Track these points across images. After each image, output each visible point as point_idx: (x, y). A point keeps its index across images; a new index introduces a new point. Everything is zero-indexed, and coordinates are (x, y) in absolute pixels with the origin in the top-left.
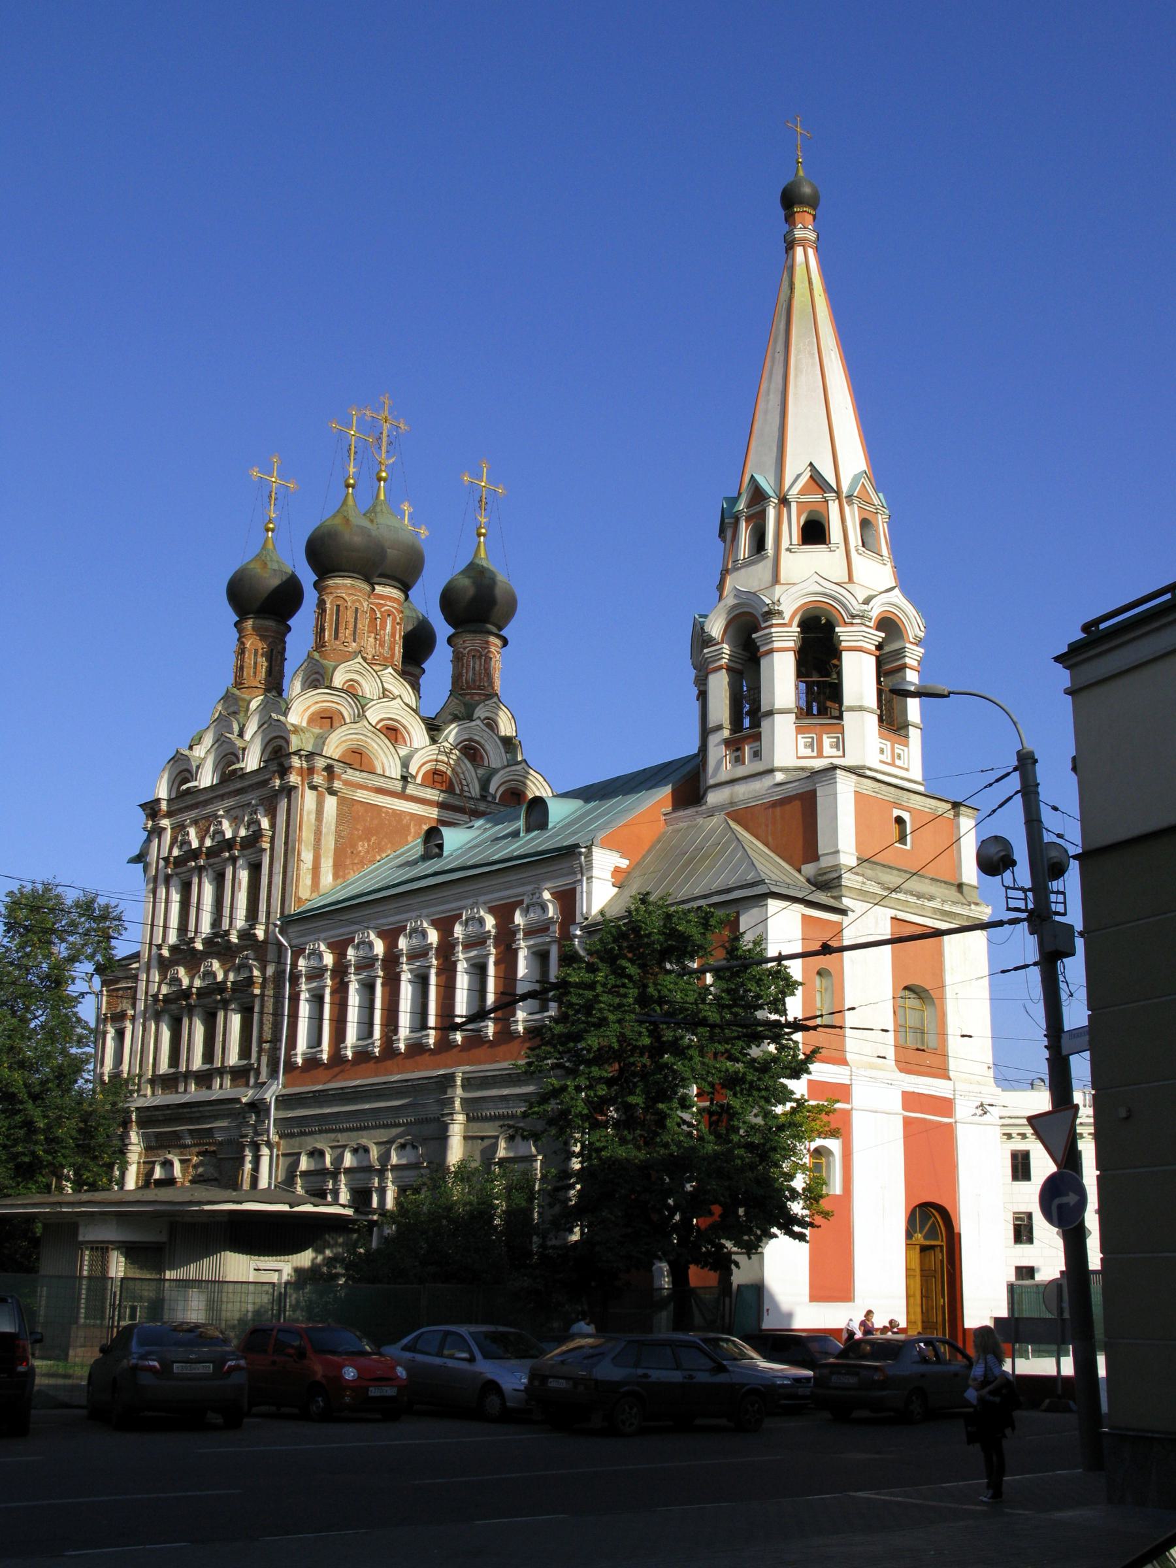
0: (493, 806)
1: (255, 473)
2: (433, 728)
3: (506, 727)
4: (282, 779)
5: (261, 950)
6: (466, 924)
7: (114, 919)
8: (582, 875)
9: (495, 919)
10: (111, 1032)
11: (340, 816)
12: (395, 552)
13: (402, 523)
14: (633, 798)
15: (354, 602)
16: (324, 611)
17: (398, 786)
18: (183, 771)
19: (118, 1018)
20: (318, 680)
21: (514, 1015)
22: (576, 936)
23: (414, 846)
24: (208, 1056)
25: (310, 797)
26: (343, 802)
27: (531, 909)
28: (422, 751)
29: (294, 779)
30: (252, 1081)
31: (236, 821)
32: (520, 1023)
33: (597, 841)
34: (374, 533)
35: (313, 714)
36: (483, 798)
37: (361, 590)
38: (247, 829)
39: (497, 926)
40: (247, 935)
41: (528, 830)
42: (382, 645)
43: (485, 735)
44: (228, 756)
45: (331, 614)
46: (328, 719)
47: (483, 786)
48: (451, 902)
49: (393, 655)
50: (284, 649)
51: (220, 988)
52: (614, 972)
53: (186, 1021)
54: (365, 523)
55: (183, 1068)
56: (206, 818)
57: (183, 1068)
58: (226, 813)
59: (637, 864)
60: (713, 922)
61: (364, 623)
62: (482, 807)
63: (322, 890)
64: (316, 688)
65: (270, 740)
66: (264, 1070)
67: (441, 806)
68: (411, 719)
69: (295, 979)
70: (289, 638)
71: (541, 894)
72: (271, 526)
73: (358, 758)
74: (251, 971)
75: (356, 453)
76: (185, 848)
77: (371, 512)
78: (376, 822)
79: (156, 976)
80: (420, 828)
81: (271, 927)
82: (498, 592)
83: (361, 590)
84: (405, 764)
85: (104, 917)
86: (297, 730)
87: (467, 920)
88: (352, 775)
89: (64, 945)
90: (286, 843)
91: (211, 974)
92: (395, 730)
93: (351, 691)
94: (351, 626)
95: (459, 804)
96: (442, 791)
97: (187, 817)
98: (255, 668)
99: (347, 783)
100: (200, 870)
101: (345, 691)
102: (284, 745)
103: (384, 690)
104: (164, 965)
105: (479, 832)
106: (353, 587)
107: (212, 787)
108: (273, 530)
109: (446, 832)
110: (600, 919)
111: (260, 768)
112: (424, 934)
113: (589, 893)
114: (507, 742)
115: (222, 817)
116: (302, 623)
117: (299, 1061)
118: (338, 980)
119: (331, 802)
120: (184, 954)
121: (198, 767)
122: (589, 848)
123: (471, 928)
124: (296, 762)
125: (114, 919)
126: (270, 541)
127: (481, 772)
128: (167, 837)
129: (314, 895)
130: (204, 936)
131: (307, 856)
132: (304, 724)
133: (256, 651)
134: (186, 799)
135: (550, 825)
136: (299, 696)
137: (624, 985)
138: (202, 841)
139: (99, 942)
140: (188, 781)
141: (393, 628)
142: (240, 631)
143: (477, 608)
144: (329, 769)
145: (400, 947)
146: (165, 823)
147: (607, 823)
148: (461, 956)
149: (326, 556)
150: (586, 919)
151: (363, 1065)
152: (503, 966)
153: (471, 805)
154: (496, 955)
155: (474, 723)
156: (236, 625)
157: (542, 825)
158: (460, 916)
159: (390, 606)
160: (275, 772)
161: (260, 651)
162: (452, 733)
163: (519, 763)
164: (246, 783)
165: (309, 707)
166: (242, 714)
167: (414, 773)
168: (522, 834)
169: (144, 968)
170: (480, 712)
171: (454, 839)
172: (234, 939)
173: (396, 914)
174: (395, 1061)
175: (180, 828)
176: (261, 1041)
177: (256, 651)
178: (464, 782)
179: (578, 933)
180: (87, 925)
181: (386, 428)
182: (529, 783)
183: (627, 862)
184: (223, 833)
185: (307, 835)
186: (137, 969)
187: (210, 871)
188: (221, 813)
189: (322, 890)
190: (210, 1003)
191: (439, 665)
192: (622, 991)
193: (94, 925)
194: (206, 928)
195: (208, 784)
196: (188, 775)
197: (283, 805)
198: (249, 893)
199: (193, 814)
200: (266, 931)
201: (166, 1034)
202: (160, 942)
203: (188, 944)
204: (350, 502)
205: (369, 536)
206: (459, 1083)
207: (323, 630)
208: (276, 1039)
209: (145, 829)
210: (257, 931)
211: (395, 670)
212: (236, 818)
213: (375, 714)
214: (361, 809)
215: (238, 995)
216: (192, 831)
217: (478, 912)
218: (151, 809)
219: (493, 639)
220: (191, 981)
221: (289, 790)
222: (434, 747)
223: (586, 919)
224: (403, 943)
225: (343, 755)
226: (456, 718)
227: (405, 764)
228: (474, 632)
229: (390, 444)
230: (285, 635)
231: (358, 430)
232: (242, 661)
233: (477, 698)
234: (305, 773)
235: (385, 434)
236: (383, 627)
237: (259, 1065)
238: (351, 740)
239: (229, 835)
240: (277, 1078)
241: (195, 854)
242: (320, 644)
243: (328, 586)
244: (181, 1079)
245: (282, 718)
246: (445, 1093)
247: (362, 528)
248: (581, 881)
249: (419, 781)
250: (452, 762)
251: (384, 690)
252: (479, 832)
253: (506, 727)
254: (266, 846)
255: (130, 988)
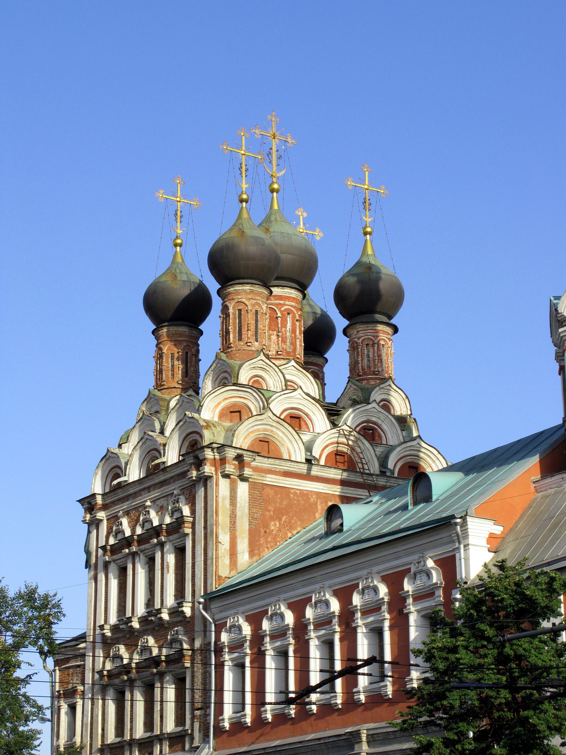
0: (393, 481)
1: (161, 195)
2: (333, 412)
3: (400, 407)
4: (198, 470)
5: (188, 624)
6: (363, 593)
7: (53, 607)
8: (459, 543)
9: (388, 587)
10: (64, 708)
11: (253, 500)
12: (290, 256)
13: (299, 227)
14: (503, 467)
15: (253, 305)
16: (228, 315)
17: (303, 469)
18: (113, 467)
19: (69, 694)
20: (226, 378)
21: (409, 674)
22: (456, 600)
23: (319, 524)
24: (149, 725)
25: (224, 485)
26: (255, 487)
27: (418, 576)
28: (324, 437)
29: (208, 469)
30: (187, 746)
31: (161, 510)
32: (415, 681)
33: (472, 511)
34: (268, 241)
35: (223, 409)
36: (383, 473)
37: (259, 294)
38: (172, 517)
39: (390, 593)
40: (176, 612)
41: (415, 503)
42: (284, 341)
43: (382, 417)
44: (152, 452)
45: (234, 318)
46: (237, 413)
47: (382, 464)
48: (348, 573)
49: (295, 350)
50: (198, 351)
51: (156, 662)
52: (474, 636)
53: (128, 696)
54: (259, 233)
55: (127, 737)
56: (136, 509)
57: (127, 737)
58: (147, 506)
59: (511, 529)
60: (556, 585)
61: (264, 323)
62: (382, 482)
63: (240, 567)
64: (225, 385)
65: (188, 435)
66: (197, 735)
67: (343, 483)
68: (312, 407)
69: (219, 651)
70: (202, 341)
71: (425, 562)
72: (179, 241)
73: (265, 446)
74: (181, 645)
75: (247, 170)
76: (120, 537)
77: (266, 224)
78: (285, 503)
79: (100, 652)
80: (327, 503)
81: (196, 604)
82: (383, 286)
83: (259, 294)
84: (309, 448)
85: (44, 606)
86: (208, 425)
87: (363, 590)
88: (260, 462)
89: (9, 633)
90: (205, 528)
91: (146, 649)
92: (299, 418)
93: (256, 386)
94: (252, 328)
95: (359, 481)
96: (344, 470)
97: (120, 509)
98: (173, 370)
99: (256, 469)
100: (134, 555)
101: (251, 387)
102: (200, 439)
103: (286, 381)
104: (107, 643)
105: (376, 506)
106: (252, 292)
107: (140, 481)
108: (181, 245)
109: (345, 509)
110: (478, 582)
111: (180, 462)
112: (327, 604)
113: (467, 559)
114: (402, 421)
115: (150, 507)
116: (211, 326)
117: (227, 725)
118: (255, 650)
119: (243, 488)
120: (124, 633)
121: (126, 464)
122: (464, 518)
123: (367, 597)
124: (209, 454)
125: (53, 607)
126: (179, 255)
127: (379, 450)
128: (104, 527)
129: (233, 573)
130: (140, 615)
131: (224, 538)
132: (216, 419)
133: (173, 355)
134: (119, 492)
135: (434, 498)
136: (210, 393)
137: (483, 646)
138: (133, 530)
139: (41, 628)
140: (119, 476)
141: (293, 325)
142: (157, 338)
143: (368, 299)
144: (239, 458)
145: (264, 628)
146: (101, 515)
147: (481, 494)
148: (360, 622)
149: (227, 265)
150: (466, 583)
151: (282, 727)
152: (396, 631)
153: (369, 481)
154: (391, 620)
155: (370, 406)
156: (154, 332)
157: (428, 498)
158: (357, 586)
159: (289, 305)
160: (191, 464)
161: (176, 355)
162: (350, 418)
163: (414, 439)
164: (168, 476)
165: (219, 404)
166: (163, 413)
167: (318, 457)
168: (410, 507)
169: (90, 645)
170: (376, 395)
171: (353, 516)
172: (165, 616)
173: (303, 586)
174: (309, 721)
175: (114, 519)
176: (193, 709)
177: (173, 355)
178: (364, 462)
179: (458, 596)
180: (30, 614)
181: (274, 144)
182: (421, 455)
183: (501, 529)
184: (151, 521)
185: (223, 519)
186: (85, 648)
187: (142, 556)
188: (148, 503)
189: (240, 567)
190: (148, 676)
191: (338, 355)
192: (482, 651)
193: (36, 614)
194: (141, 610)
195: (136, 478)
196: (119, 471)
197: (201, 492)
198: (176, 574)
199: (125, 506)
200: (193, 608)
201: (112, 707)
202: (103, 623)
203: (126, 623)
204: (245, 215)
205: (263, 245)
206: (364, 738)
207: (228, 333)
208: (206, 706)
209: (84, 521)
210: (184, 609)
211: (297, 363)
212: (162, 507)
213: (278, 406)
214: (271, 492)
215: (172, 668)
216: (125, 521)
217: (324, 595)
218: (88, 503)
219: (381, 327)
220: (131, 659)
221: (205, 480)
222: (334, 431)
223: (466, 583)
224: (309, 613)
225: (252, 445)
226: (355, 403)
227: (309, 448)
228: (366, 323)
229: (279, 157)
230: (198, 339)
231: (247, 149)
232: (161, 364)
233: (372, 382)
234: (218, 463)
235: (274, 149)
236: (284, 325)
237: (192, 730)
238: (258, 430)
239: (156, 523)
240: (208, 742)
241: (128, 542)
242: (226, 346)
243: (229, 293)
244: (127, 747)
245: (196, 416)
246: (353, 749)
247: (256, 238)
248: (458, 548)
249: (322, 462)
250: (350, 443)
251: (286, 381)
252: (376, 506)
253: (400, 407)
254: (188, 531)
255: (79, 666)
